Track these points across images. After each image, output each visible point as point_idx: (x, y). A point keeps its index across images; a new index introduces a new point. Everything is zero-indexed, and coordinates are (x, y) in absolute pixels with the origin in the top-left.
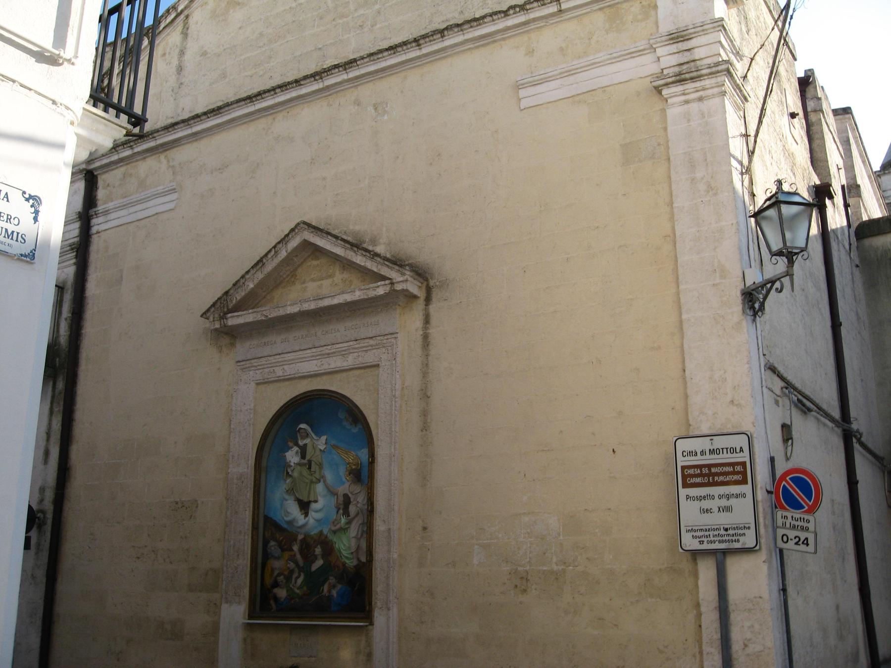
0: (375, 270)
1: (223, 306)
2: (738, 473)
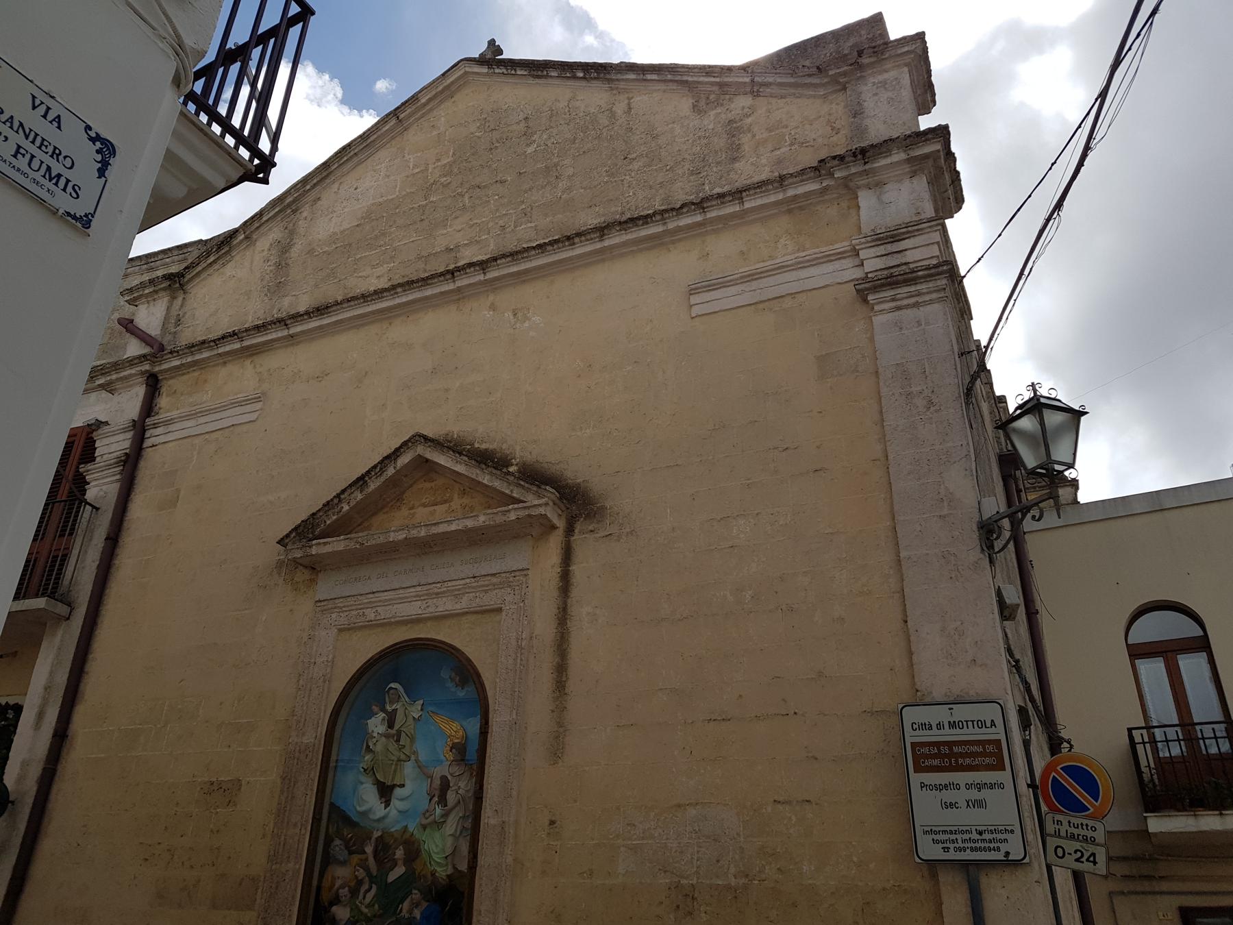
0: (507, 492)
1: (306, 531)
2: (990, 755)
